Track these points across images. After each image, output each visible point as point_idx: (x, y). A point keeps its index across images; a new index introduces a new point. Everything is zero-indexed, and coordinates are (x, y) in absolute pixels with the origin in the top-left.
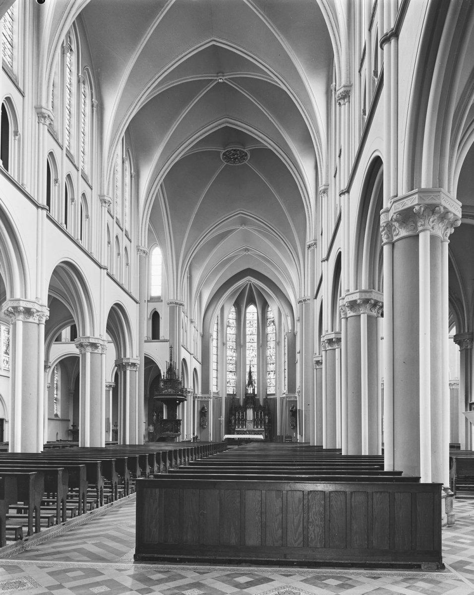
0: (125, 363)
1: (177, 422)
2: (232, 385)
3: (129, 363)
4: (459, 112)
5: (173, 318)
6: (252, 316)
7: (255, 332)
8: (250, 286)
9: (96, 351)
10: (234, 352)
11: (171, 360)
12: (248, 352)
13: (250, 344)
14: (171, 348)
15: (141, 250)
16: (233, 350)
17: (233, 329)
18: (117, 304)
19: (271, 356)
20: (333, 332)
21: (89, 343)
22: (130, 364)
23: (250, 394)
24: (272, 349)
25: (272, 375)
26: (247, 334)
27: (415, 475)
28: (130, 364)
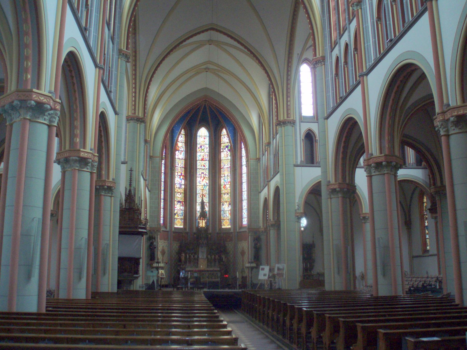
0: (108, 186)
1: (235, 343)
3: (103, 186)
5: (117, 143)
6: (202, 139)
8: (205, 108)
9: (450, 125)
10: (183, 179)
11: (130, 185)
12: (198, 179)
14: (131, 171)
15: (123, 54)
16: (182, 177)
17: (182, 153)
19: (225, 185)
20: (383, 155)
21: (78, 157)
22: (106, 187)
23: (202, 228)
26: (198, 159)
27: (137, 256)
28: (106, 187)
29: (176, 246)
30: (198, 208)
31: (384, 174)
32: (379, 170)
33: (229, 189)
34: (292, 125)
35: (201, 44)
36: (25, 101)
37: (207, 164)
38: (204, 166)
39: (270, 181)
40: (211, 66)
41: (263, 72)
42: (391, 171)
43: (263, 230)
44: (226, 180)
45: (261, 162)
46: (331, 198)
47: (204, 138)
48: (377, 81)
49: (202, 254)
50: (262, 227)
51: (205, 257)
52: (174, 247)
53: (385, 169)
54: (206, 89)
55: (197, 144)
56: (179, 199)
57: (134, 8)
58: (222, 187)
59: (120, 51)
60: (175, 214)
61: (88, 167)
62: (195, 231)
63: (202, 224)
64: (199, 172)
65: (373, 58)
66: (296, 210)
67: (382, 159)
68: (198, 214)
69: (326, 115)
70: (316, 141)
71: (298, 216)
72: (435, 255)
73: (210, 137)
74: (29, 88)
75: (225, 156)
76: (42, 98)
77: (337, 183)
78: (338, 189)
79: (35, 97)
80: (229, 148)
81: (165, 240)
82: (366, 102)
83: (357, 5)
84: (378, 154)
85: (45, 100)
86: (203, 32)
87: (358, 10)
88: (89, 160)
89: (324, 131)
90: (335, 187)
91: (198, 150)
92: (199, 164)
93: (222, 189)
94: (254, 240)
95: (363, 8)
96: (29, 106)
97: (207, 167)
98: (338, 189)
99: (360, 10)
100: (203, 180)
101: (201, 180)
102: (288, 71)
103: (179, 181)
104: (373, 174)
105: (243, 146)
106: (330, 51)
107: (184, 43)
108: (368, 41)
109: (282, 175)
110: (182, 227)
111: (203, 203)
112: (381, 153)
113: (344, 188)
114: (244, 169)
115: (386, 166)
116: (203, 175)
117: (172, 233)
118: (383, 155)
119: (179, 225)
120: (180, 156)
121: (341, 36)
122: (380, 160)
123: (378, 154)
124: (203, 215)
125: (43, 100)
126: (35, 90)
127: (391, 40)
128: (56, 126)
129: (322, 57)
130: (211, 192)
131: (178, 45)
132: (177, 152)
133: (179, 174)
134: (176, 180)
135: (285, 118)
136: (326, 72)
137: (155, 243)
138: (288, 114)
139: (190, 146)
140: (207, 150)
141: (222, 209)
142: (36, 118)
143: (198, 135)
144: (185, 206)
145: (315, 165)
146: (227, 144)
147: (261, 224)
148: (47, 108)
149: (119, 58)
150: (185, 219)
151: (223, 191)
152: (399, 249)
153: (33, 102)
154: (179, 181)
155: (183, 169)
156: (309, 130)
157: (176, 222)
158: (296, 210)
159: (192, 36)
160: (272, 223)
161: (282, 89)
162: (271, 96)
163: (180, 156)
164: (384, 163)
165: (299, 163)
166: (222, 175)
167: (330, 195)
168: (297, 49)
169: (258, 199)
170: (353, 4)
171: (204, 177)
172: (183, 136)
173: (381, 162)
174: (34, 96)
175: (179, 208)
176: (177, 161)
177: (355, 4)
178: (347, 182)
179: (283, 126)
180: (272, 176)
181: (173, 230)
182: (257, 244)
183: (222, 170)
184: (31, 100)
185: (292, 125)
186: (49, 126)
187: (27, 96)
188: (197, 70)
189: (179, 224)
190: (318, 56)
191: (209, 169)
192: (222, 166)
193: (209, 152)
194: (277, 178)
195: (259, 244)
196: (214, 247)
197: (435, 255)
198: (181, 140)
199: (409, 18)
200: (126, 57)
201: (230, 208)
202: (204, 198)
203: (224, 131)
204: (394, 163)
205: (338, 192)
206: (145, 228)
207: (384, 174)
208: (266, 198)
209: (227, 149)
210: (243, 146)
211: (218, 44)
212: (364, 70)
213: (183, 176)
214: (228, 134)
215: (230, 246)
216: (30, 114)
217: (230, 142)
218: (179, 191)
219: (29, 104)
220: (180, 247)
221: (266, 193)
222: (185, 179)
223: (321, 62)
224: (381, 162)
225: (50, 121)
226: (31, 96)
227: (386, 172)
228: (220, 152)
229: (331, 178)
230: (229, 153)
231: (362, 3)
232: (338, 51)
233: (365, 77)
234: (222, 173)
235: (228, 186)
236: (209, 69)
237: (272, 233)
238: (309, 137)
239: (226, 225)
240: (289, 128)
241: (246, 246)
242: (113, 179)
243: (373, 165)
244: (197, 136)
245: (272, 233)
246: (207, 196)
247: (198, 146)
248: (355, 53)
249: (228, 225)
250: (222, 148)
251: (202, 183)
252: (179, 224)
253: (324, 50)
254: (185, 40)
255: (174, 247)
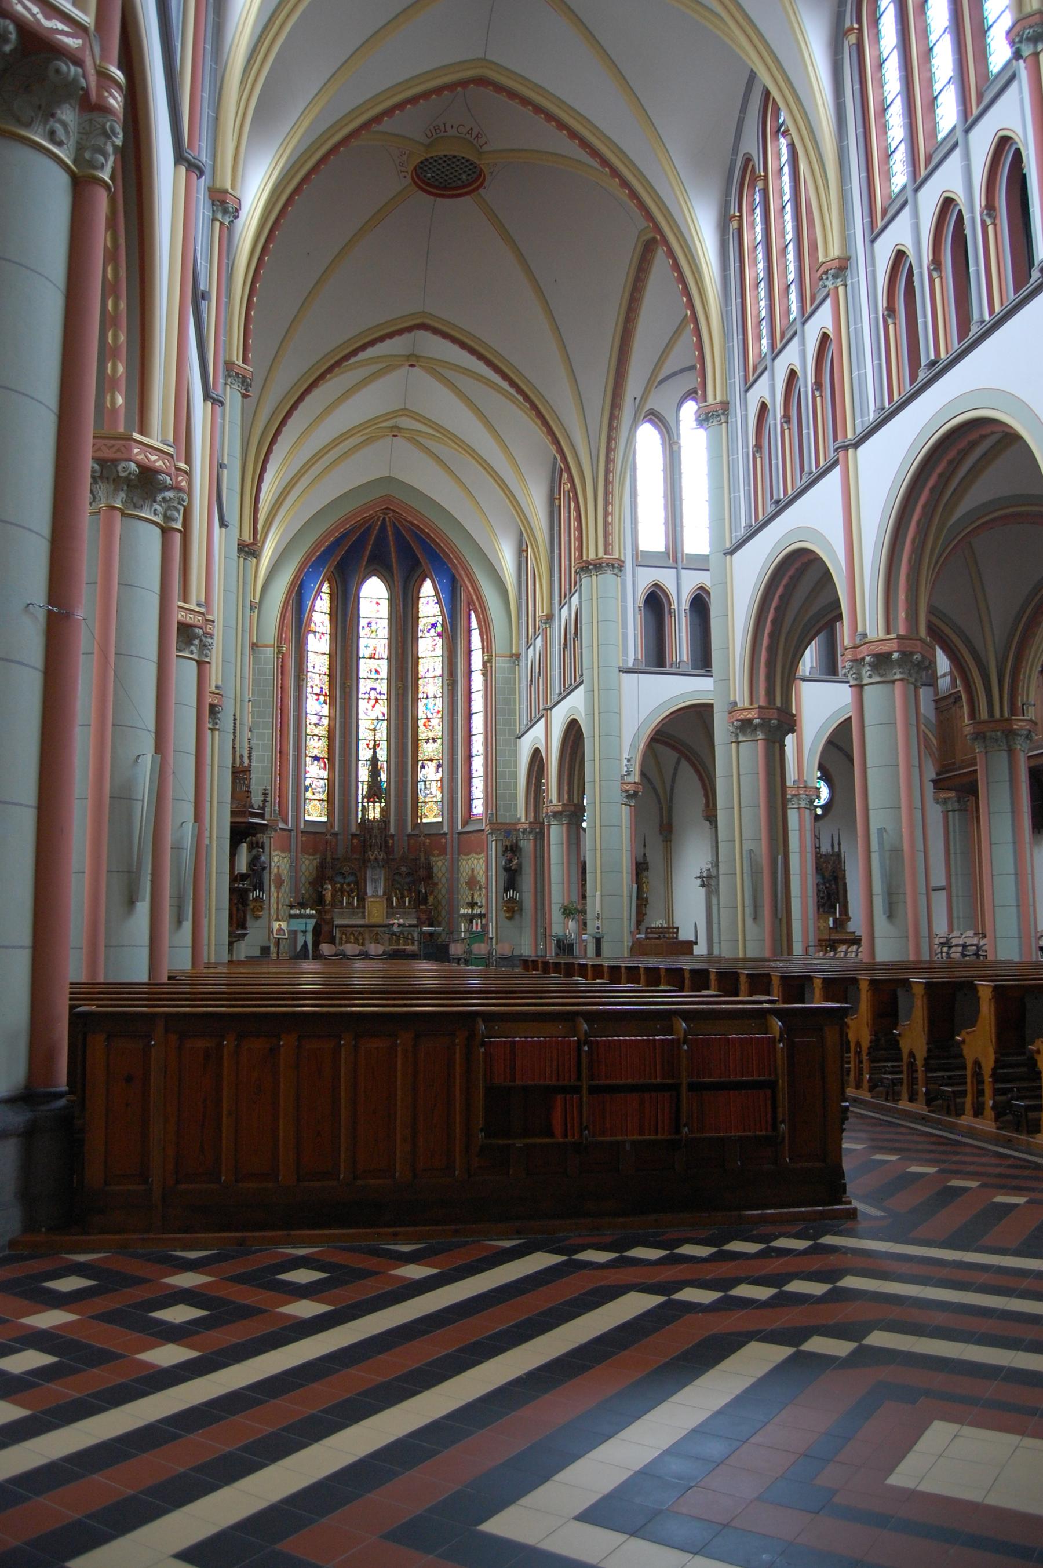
2: (318, 796)
4: (275, 203)
7: (383, 651)
8: (383, 528)
12: (363, 705)
13: (371, 684)
15: (237, 373)
16: (322, 698)
18: (701, 588)
19: (428, 719)
23: (375, 820)
24: (430, 700)
25: (431, 767)
29: (308, 865)
30: (364, 774)
31: (893, 682)
32: (882, 672)
33: (439, 728)
34: (616, 571)
35: (390, 365)
36: (115, 462)
37: (383, 667)
38: (377, 672)
39: (551, 709)
40: (405, 422)
41: (547, 440)
42: (910, 675)
43: (526, 826)
44: (430, 706)
45: (523, 664)
46: (738, 743)
47: (378, 603)
48: (885, 463)
49: (375, 888)
50: (523, 820)
51: (381, 892)
52: (304, 868)
53: (897, 670)
54: (389, 480)
55: (359, 617)
56: (316, 752)
57: (260, 259)
58: (421, 723)
59: (229, 365)
60: (306, 790)
61: (193, 648)
62: (354, 829)
63: (374, 812)
64: (364, 686)
65: (872, 407)
66: (622, 777)
67: (892, 646)
68: (363, 789)
69: (728, 545)
70: (670, 613)
71: (627, 791)
72: (935, 889)
73: (391, 600)
74: (122, 429)
75: (430, 651)
76: (154, 458)
77: (756, 706)
78: (756, 721)
79: (138, 454)
80: (439, 629)
81: (283, 851)
82: (851, 514)
83: (835, 277)
84: (882, 635)
85: (160, 463)
86: (400, 332)
87: (837, 288)
88: (197, 630)
89: (725, 582)
90: (750, 716)
91: (362, 633)
92: (365, 667)
93: (422, 728)
94: (505, 851)
95: (849, 283)
96: (123, 474)
97: (384, 674)
98: (756, 721)
99: (841, 290)
100: (373, 706)
101: (370, 707)
102: (610, 439)
103: (316, 709)
104: (866, 681)
105: (474, 624)
106: (742, 389)
107: (353, 360)
108: (861, 365)
109: (590, 692)
110: (324, 819)
111: (374, 761)
112: (888, 633)
113: (771, 719)
114: (477, 681)
115: (900, 663)
116: (373, 694)
117: (300, 835)
118: (893, 636)
119: (315, 815)
120: (318, 647)
121: (776, 353)
122: (885, 648)
123: (882, 635)
124: (375, 792)
125: (155, 461)
126: (136, 436)
127: (933, 364)
128: (179, 531)
129: (721, 402)
130: (393, 735)
131: (338, 364)
132: (311, 636)
133: (317, 690)
134: (308, 706)
135: (601, 554)
136: (731, 440)
137: (263, 858)
138: (606, 544)
139: (344, 621)
140: (382, 629)
141: (420, 776)
142: (135, 507)
143: (361, 595)
144: (331, 769)
145: (667, 669)
146: (433, 620)
147: (521, 813)
148: (164, 482)
149: (226, 384)
150: (330, 800)
151: (423, 733)
152: (922, 854)
153: (133, 466)
154: (316, 709)
155: (326, 678)
156: (656, 585)
157: (309, 807)
158: (622, 777)
159: (372, 343)
160: (556, 809)
161: (581, 488)
162: (557, 502)
163: (318, 647)
164: (895, 656)
165: (630, 665)
166: (420, 695)
167: (737, 735)
168: (633, 387)
169: (515, 754)
170: (826, 272)
171: (377, 700)
172: (326, 597)
173: (890, 654)
174: (136, 451)
175: (316, 774)
176: (311, 657)
177: (831, 272)
178: (778, 704)
179: (593, 572)
180: (556, 698)
181: (302, 826)
182: (510, 861)
183: (420, 681)
184: (130, 460)
185: (616, 571)
186: (165, 531)
187: (118, 450)
188: (388, 428)
189: (315, 813)
190: (710, 400)
191: (389, 680)
192: (421, 673)
193: (390, 639)
194: (574, 705)
195: (516, 862)
196: (403, 869)
197: (935, 889)
198: (322, 604)
199: (981, 311)
200: (243, 383)
201: (439, 776)
202: (378, 750)
203: (427, 588)
204: (917, 657)
205: (755, 728)
206: (261, 816)
207: (893, 682)
208: (537, 751)
209: (432, 630)
210: (474, 624)
211: (435, 368)
212: (850, 436)
213: (325, 695)
214: (437, 595)
215: (440, 865)
216: (122, 495)
217: (443, 614)
218: (316, 731)
219: (125, 469)
220: (322, 867)
221: (544, 736)
222: (331, 704)
223: (718, 416)
224: (890, 654)
225: (167, 518)
226: (129, 449)
227: (898, 677)
228: (415, 639)
229: (740, 694)
230: (439, 642)
231: (848, 272)
232: (768, 389)
233: (851, 451)
234: (421, 688)
235: (435, 722)
236: (399, 429)
237: (556, 833)
238: (655, 602)
239: (431, 815)
240: (608, 578)
241: (482, 866)
242: (217, 687)
243: (868, 659)
244: (359, 598)
245: (556, 833)
246: (384, 745)
247: (363, 622)
248: (817, 393)
249: (435, 816)
250: (421, 627)
251: (372, 716)
252: (315, 813)
253: (727, 386)
254: (355, 353)
255: (304, 868)
